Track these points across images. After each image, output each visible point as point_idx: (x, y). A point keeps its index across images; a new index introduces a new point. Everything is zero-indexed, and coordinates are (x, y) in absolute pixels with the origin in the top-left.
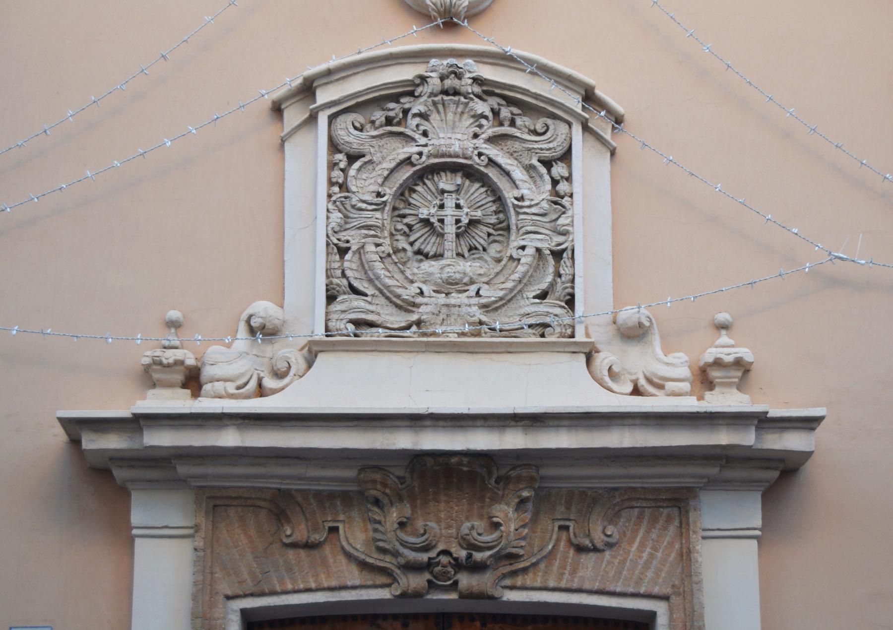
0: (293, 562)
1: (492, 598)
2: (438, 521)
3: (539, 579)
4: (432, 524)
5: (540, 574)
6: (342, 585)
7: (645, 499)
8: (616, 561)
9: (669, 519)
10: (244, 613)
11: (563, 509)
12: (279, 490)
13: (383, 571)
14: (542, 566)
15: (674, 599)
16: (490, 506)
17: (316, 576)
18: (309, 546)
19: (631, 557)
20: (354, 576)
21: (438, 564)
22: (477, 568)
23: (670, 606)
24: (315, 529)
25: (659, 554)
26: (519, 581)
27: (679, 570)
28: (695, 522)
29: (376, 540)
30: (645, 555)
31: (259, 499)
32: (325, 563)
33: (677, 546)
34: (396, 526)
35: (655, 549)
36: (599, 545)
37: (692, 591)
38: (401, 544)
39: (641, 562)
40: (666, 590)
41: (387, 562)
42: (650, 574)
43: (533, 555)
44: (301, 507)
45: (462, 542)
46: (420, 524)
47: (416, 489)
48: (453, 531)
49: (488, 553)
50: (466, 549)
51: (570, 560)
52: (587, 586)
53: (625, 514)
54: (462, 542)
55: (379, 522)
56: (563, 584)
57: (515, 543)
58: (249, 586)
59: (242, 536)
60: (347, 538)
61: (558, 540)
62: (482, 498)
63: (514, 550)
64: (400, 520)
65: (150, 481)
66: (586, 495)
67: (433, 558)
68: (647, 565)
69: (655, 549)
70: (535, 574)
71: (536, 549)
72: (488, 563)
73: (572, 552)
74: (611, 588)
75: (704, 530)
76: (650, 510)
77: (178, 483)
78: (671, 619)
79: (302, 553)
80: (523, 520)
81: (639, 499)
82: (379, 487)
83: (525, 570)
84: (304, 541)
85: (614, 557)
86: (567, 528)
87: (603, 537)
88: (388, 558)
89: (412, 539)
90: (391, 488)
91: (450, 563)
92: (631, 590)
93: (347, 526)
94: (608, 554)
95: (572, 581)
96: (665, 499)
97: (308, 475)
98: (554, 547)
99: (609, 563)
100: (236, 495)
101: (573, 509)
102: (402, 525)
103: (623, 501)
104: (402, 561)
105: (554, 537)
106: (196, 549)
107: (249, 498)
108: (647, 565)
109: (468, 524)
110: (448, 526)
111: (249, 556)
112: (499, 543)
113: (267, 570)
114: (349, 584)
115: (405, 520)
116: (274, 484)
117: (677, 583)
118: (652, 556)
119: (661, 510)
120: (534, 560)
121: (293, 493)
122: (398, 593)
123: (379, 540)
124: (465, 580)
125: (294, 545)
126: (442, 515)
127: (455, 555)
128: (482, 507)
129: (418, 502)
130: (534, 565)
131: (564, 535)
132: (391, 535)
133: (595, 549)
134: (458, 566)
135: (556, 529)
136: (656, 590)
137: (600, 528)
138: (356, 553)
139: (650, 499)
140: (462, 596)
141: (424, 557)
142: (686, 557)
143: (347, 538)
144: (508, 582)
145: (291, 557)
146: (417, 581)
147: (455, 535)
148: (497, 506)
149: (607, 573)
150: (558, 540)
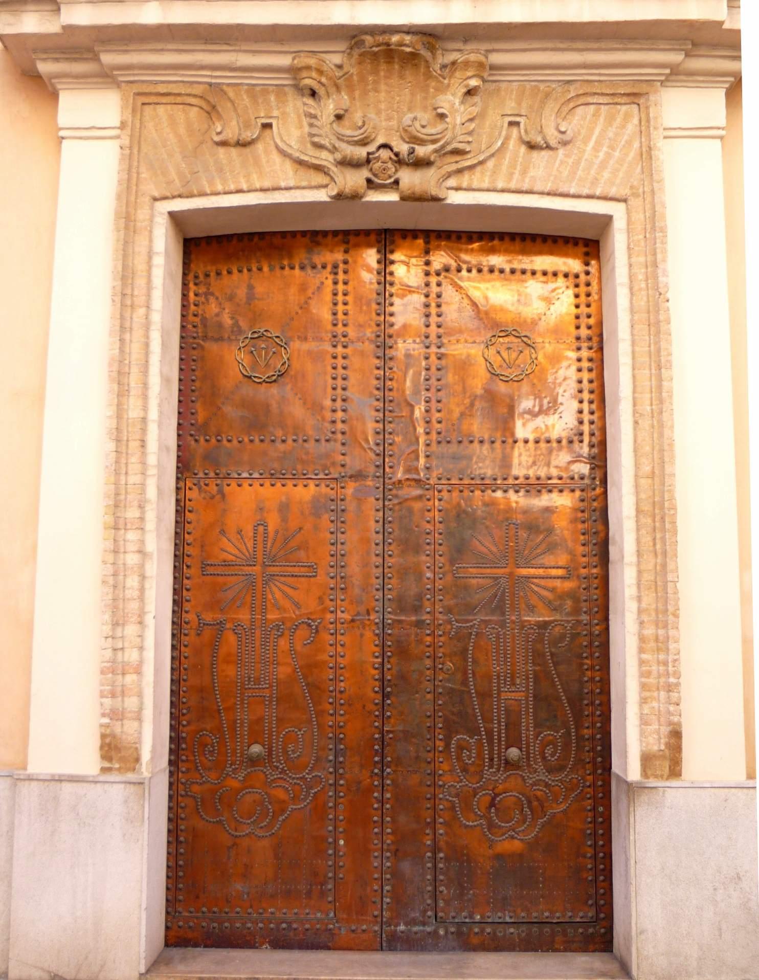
0: (224, 162)
1: (436, 199)
2: (379, 113)
3: (487, 180)
4: (372, 115)
5: (488, 173)
6: (275, 186)
7: (603, 94)
8: (570, 161)
9: (627, 117)
10: (171, 214)
11: (513, 104)
12: (210, 84)
13: (318, 168)
14: (490, 164)
15: (632, 202)
16: (434, 97)
17: (247, 176)
18: (242, 144)
19: (586, 156)
20: (286, 174)
21: (378, 159)
22: (421, 164)
23: (627, 209)
24: (247, 125)
25: (617, 154)
26: (465, 180)
27: (639, 169)
28: (656, 118)
29: (312, 135)
30: (601, 155)
31: (189, 95)
32: (257, 162)
33: (636, 145)
34: (332, 118)
35: (612, 148)
36: (553, 143)
37: (653, 191)
38: (338, 138)
39: (598, 161)
40: (624, 192)
41: (325, 158)
42: (606, 174)
43: (481, 152)
44: (232, 102)
45: (403, 134)
46: (358, 117)
47: (355, 78)
48: (394, 123)
49: (431, 147)
50: (408, 143)
51: (520, 159)
52: (538, 187)
53: (580, 111)
54: (403, 134)
55: (315, 117)
56: (513, 185)
57: (461, 138)
58: (178, 186)
59: (171, 136)
60: (280, 135)
61: (507, 138)
62: (425, 89)
63: (461, 146)
64: (337, 112)
65: (77, 77)
66: (539, 90)
67: (373, 153)
68: (603, 166)
69: (612, 148)
70: (482, 173)
71: (483, 147)
72: (432, 159)
73: (523, 149)
74: (564, 189)
75: (665, 129)
76: (607, 107)
77: (107, 78)
78: (629, 222)
79: (234, 151)
80: (470, 114)
81: (595, 94)
82: (314, 74)
83: (471, 168)
84: (236, 138)
85: (567, 156)
86: (517, 124)
87: (556, 133)
88: (324, 154)
89: (349, 132)
90: (327, 77)
91: (390, 158)
92: (585, 191)
93: (280, 122)
94: (561, 152)
95: (523, 181)
96: (624, 94)
97: (239, 64)
98: (503, 144)
99: (562, 162)
100: (165, 91)
101: (524, 105)
102: (339, 117)
103: (578, 96)
104: (338, 156)
105: (504, 133)
106: (121, 148)
107: (179, 95)
108: (603, 166)
109: (411, 116)
110: (389, 112)
111: (178, 157)
112: (444, 137)
113: (196, 170)
114: (283, 184)
115: (342, 112)
116: (205, 77)
117: (635, 183)
118: (608, 156)
119: (619, 107)
120: (481, 158)
121: (225, 87)
122: (334, 193)
123: (314, 135)
124: (409, 179)
125: (224, 144)
126: (383, 106)
127: (396, 150)
128: (425, 98)
129: (357, 93)
130: (481, 163)
131: (515, 130)
132: (327, 129)
133: (548, 147)
134: (399, 161)
135: (506, 125)
136: (613, 192)
137: (553, 125)
138: (289, 151)
139: (607, 95)
140: (403, 199)
141: (362, 152)
142: (647, 155)
143: (280, 135)
144: (452, 182)
145: (222, 156)
146: (354, 180)
147: (396, 127)
148: (441, 97)
149: (561, 173)
150: (507, 138)
